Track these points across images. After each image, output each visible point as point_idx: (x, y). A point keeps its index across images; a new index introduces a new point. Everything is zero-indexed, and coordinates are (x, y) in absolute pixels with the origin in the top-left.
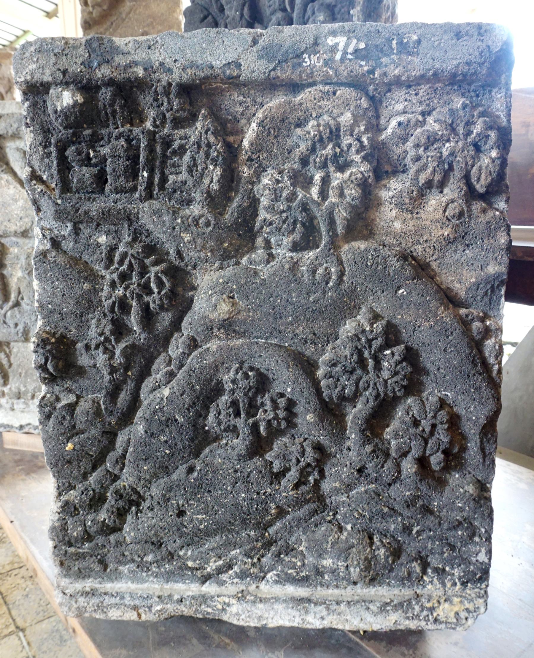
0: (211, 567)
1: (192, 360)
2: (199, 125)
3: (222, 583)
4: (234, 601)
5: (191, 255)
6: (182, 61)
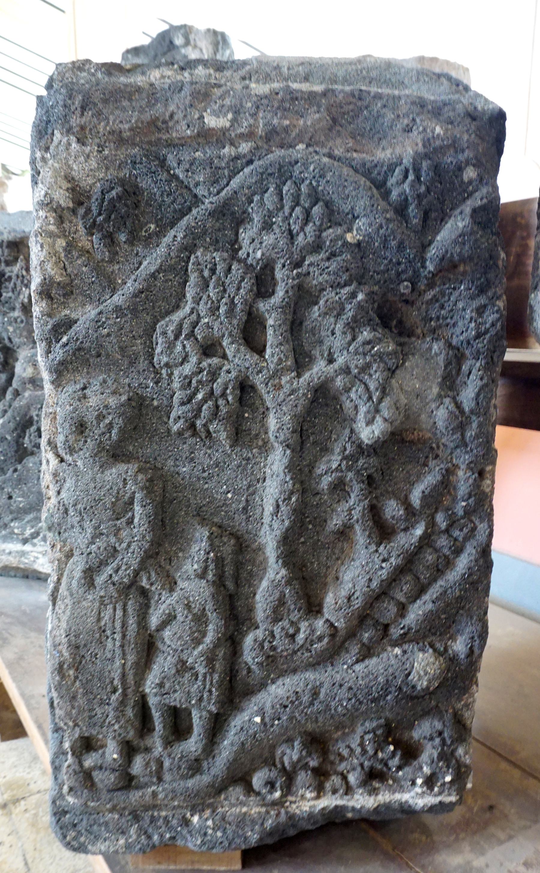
0: (29, 532)
1: (16, 404)
2: (18, 265)
3: (34, 545)
4: (40, 556)
5: (16, 340)
6: (8, 228)
